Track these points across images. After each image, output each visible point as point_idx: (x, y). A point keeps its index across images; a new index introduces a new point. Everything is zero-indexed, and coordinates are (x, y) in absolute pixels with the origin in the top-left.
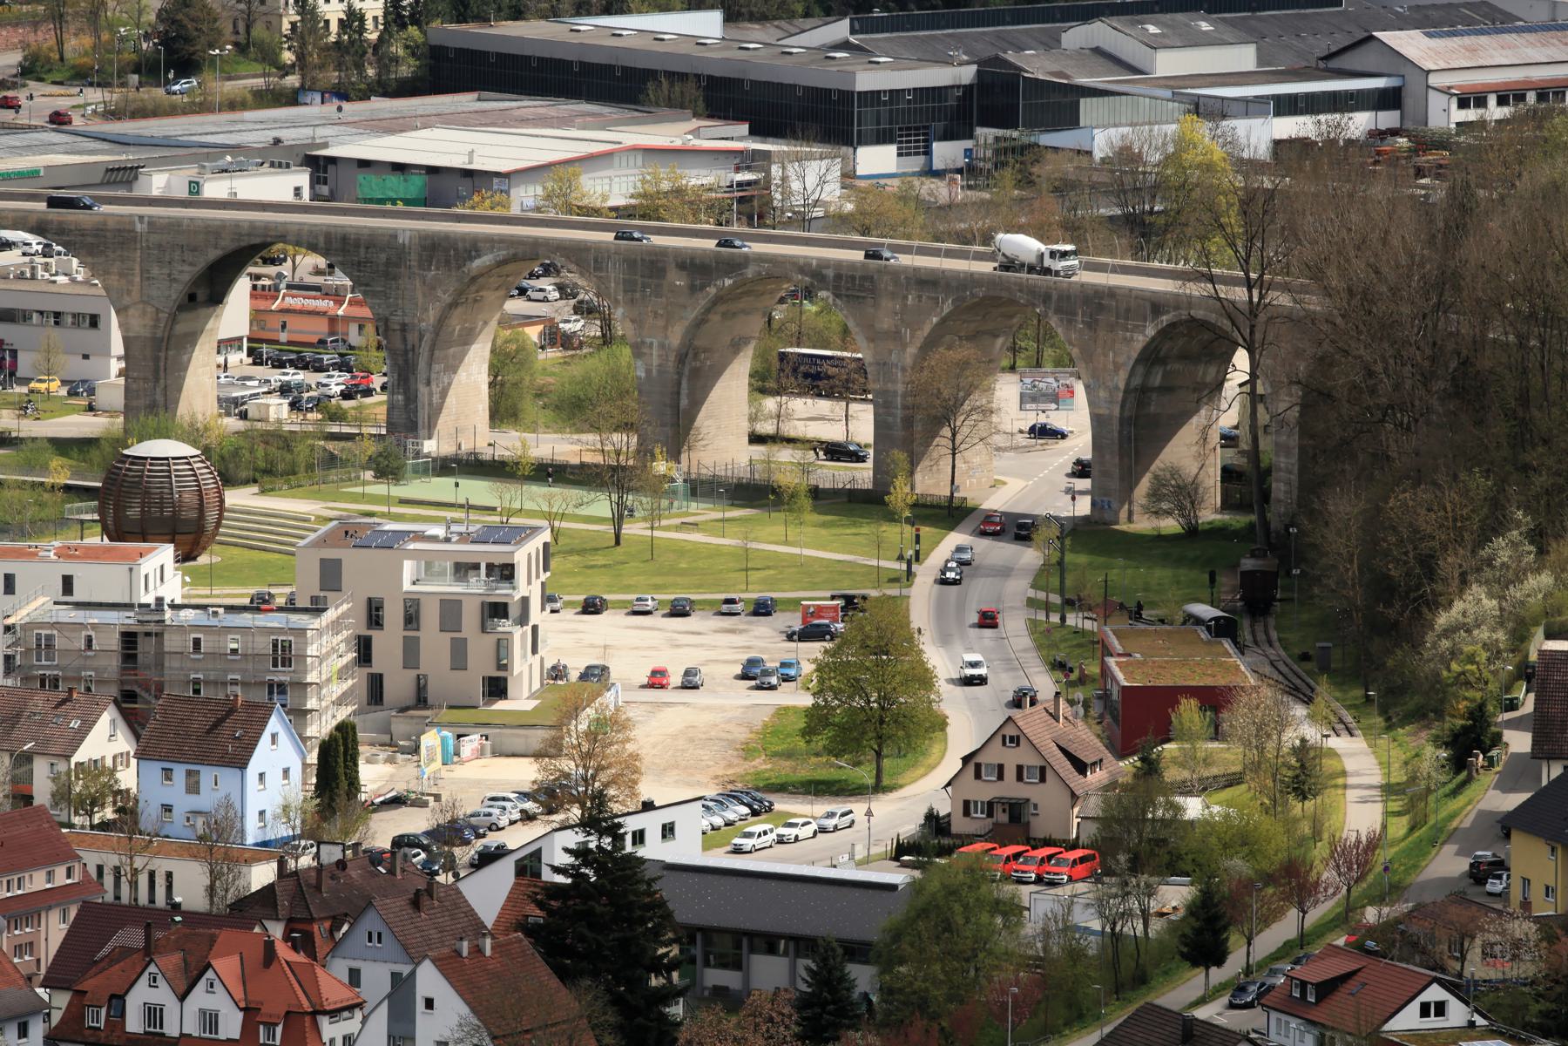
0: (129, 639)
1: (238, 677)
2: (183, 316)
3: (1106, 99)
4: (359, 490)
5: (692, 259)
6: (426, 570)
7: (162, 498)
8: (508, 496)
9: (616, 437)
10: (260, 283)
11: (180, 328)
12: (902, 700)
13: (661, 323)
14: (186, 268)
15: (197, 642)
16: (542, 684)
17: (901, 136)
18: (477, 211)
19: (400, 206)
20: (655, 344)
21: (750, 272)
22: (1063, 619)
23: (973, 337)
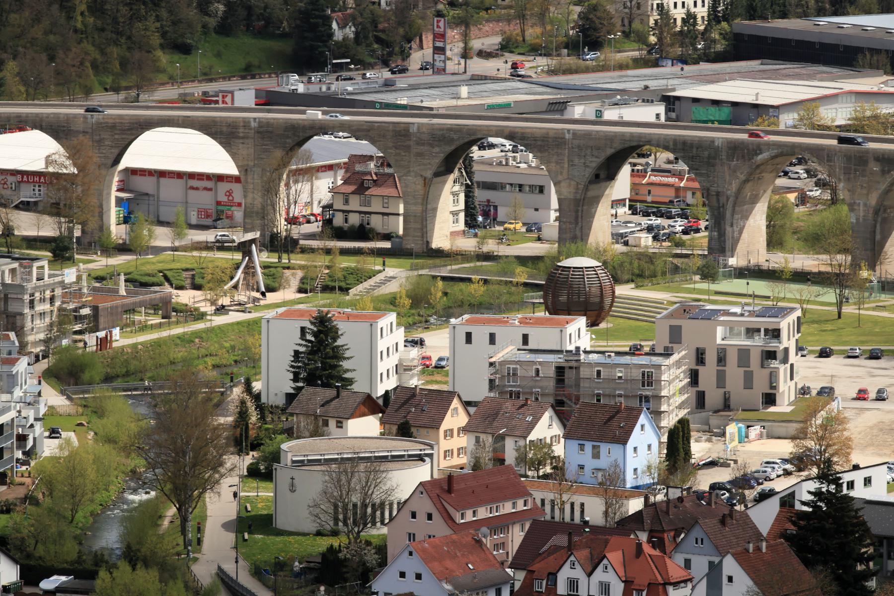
0: (560, 370)
1: (622, 393)
4: (692, 286)
5: (883, 155)
11: (590, 194)
13: (865, 192)
14: (594, 159)
15: (599, 372)
16: (796, 397)
19: (716, 125)
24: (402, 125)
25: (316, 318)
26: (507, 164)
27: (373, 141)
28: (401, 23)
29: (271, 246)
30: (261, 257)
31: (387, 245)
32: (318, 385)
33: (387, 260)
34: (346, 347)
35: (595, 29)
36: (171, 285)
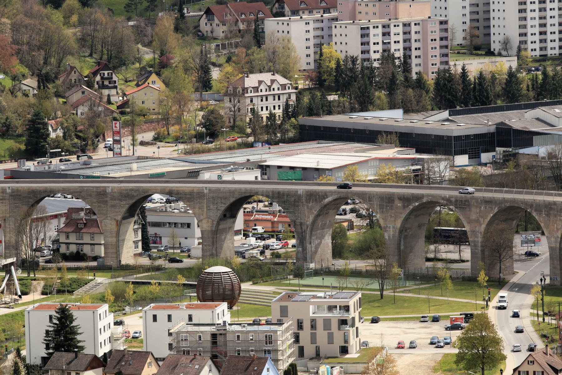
0: (214, 336)
1: (254, 349)
2: (222, 222)
3: (542, 136)
4: (288, 282)
5: (404, 196)
6: (318, 308)
7: (219, 285)
9: (380, 260)
10: (246, 210)
11: (221, 227)
12: (490, 349)
13: (393, 219)
14: (223, 205)
15: (238, 337)
16: (360, 348)
17: (470, 151)
18: (322, 182)
19: (294, 181)
20: (391, 227)
21: (425, 200)
22: (544, 319)
23: (505, 221)
24: (102, 188)
25: (59, 309)
26: (166, 211)
27: (84, 199)
28: (91, 126)
29: (23, 267)
30: (17, 274)
31: (94, 264)
32: (62, 351)
33: (96, 274)
34: (78, 327)
35: (213, 126)
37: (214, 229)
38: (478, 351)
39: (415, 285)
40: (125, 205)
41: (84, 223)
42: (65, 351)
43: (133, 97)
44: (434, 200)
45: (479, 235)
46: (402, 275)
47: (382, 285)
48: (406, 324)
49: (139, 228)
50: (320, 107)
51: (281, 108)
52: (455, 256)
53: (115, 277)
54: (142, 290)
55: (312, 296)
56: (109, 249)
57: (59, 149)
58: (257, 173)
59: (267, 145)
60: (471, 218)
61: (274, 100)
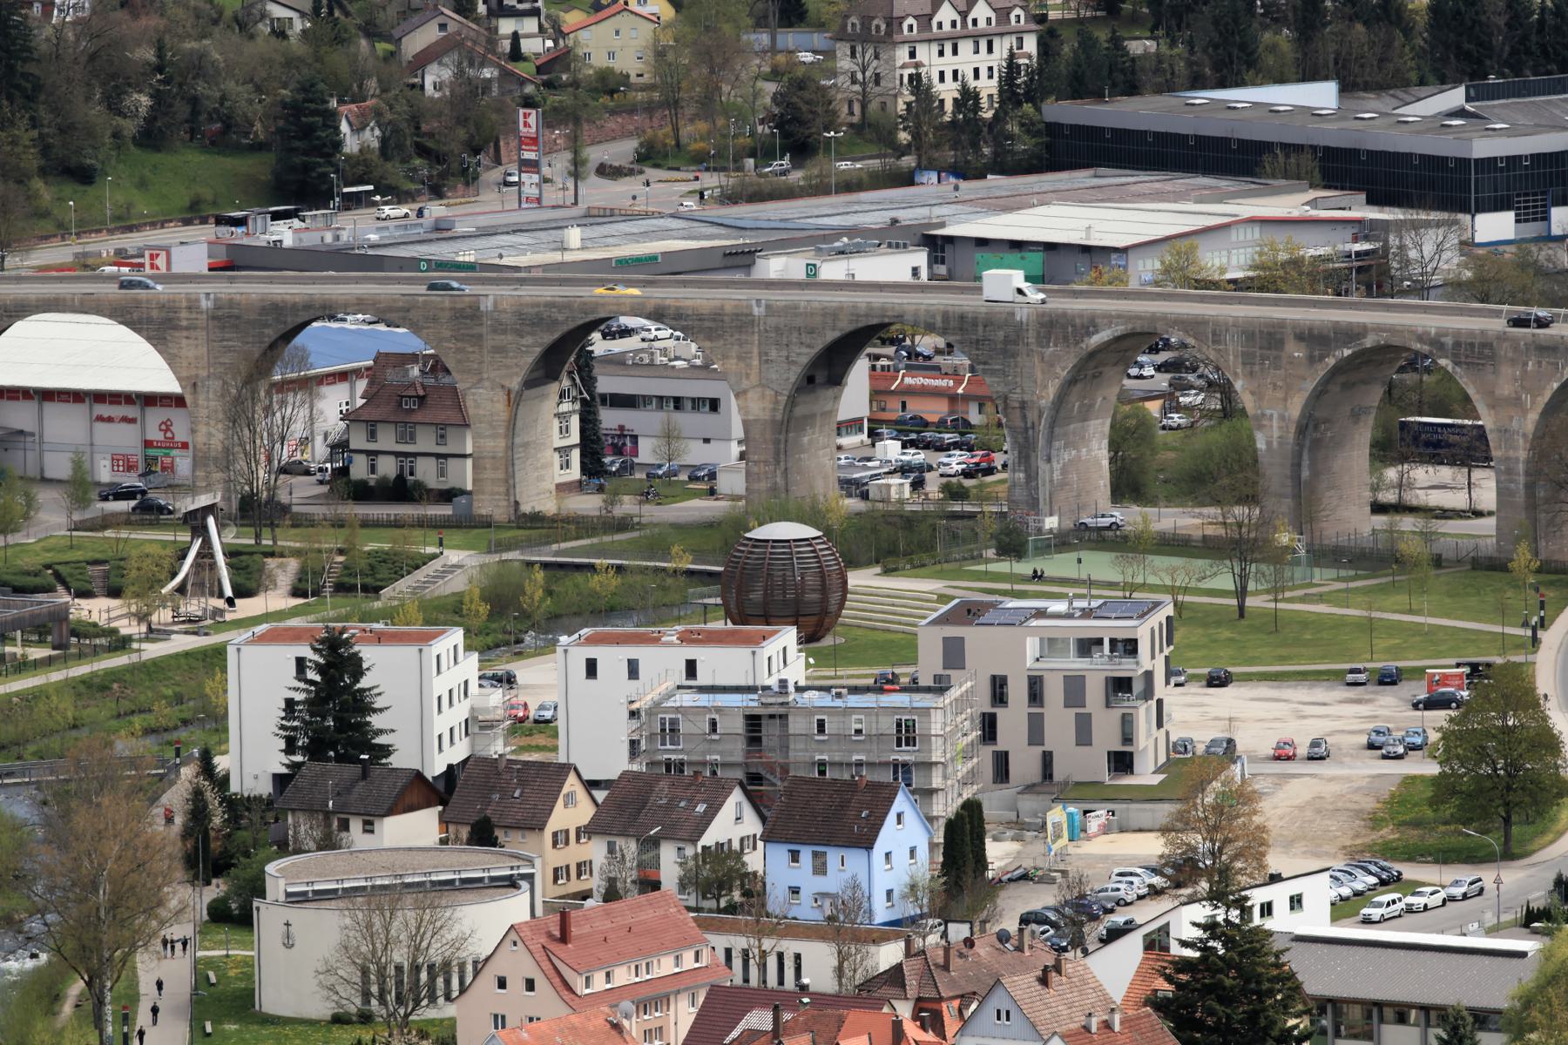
0: (753, 722)
4: (982, 568)
5: (1310, 329)
8: (1130, 571)
11: (799, 411)
12: (1528, 766)
13: (1280, 394)
15: (821, 724)
17: (1519, 202)
20: (1275, 416)
21: (1369, 342)
25: (322, 642)
27: (415, 328)
31: (445, 510)
32: (329, 759)
35: (802, 123)
36: (68, 589)
37: (779, 417)
38: (1495, 770)
39: (1338, 579)
40: (532, 347)
41: (418, 397)
42: (340, 759)
43: (576, 42)
44: (1396, 341)
45: (1521, 441)
46: (1303, 552)
47: (1243, 578)
48: (1305, 691)
49: (574, 411)
50: (1105, 72)
51: (996, 74)
52: (1458, 500)
53: (501, 547)
54: (569, 585)
55: (1033, 612)
56: (485, 469)
57: (368, 183)
58: (920, 258)
59: (952, 180)
60: (1498, 392)
61: (977, 52)
